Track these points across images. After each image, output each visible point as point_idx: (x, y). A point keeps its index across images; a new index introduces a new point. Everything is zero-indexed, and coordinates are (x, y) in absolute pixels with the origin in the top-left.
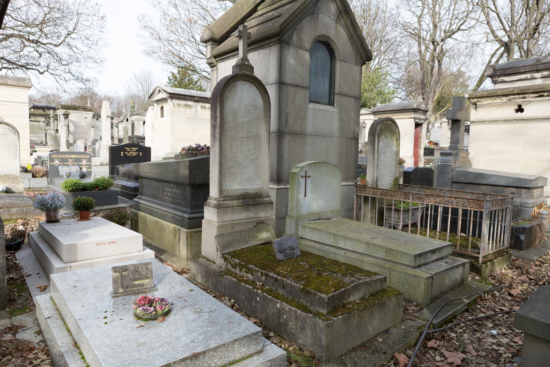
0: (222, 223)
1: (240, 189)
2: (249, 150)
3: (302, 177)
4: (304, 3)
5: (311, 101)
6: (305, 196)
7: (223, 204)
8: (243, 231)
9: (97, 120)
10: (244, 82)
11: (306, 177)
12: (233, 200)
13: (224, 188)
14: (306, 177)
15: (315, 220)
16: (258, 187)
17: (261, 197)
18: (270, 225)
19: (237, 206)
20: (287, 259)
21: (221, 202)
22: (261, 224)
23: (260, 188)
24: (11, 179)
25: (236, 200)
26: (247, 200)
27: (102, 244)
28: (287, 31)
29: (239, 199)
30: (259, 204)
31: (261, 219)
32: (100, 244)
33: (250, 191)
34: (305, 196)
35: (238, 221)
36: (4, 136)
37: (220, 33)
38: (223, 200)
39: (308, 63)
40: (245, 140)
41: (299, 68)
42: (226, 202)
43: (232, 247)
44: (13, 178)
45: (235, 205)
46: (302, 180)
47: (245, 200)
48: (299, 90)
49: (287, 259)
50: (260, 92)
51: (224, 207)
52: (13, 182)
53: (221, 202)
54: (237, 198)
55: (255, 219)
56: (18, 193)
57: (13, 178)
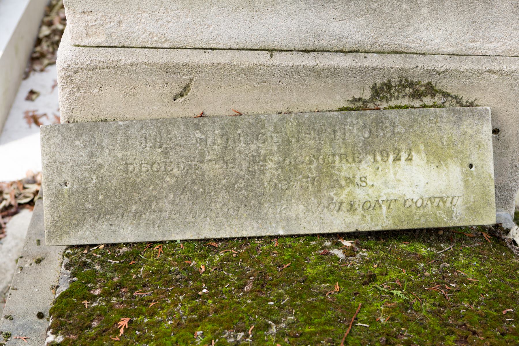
0: (101, 55)
18: (481, 116)
22: (417, 95)
31: (420, 62)
35: (225, 58)
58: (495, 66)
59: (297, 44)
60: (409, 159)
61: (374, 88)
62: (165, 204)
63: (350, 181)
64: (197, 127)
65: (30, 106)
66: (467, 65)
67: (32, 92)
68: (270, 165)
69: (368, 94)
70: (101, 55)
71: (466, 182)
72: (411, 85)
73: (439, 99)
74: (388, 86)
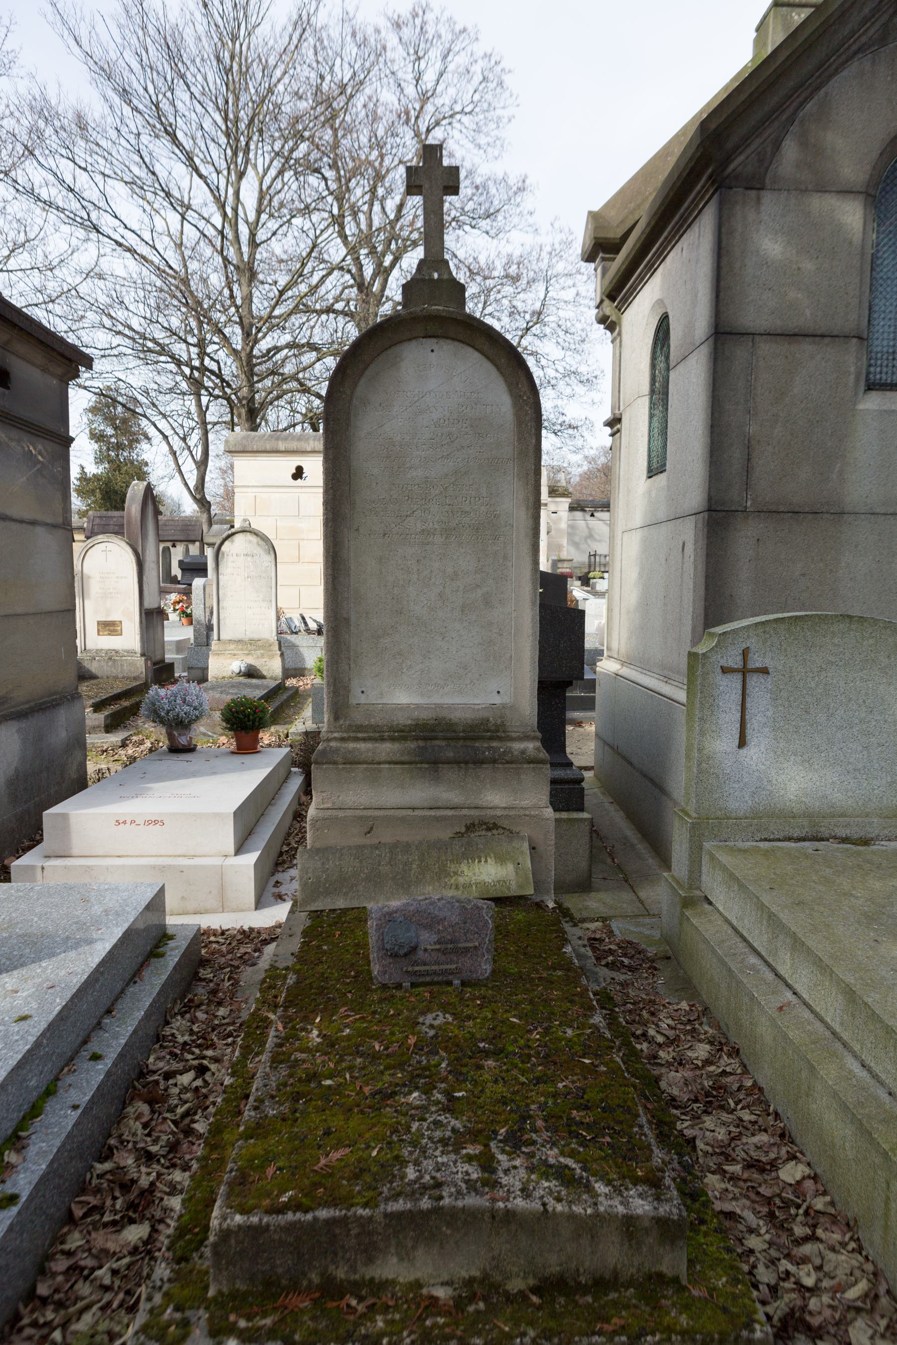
0: (329, 813)
1: (418, 707)
2: (456, 574)
3: (725, 670)
4: (842, 5)
5: (871, 387)
6: (742, 743)
7: (337, 750)
8: (408, 845)
9: (592, 515)
10: (431, 343)
11: (745, 672)
12: (382, 739)
13: (357, 698)
14: (745, 672)
15: (789, 839)
16: (497, 700)
17: (500, 739)
18: (523, 838)
19: (389, 763)
20: (413, 985)
21: (333, 744)
22: (489, 829)
23: (504, 706)
24: (259, 648)
25: (393, 739)
26: (437, 742)
27: (128, 822)
28: (746, 140)
29: (405, 738)
30: (482, 762)
31: (490, 813)
32: (125, 822)
33: (456, 716)
34: (742, 743)
35: (391, 812)
36: (249, 559)
37: (626, 217)
38: (342, 739)
39: (857, 237)
40: (438, 539)
41: (808, 266)
42: (351, 745)
43: (346, 894)
44: (263, 647)
45: (383, 757)
46: (729, 687)
47: (429, 743)
48: (807, 347)
49: (413, 985)
50: (498, 368)
51: (340, 760)
52: (262, 656)
53: (333, 744)
54: (399, 734)
55: (465, 812)
56: (271, 678)
57: (263, 647)
58: (527, 813)
59: (426, 805)
60: (486, 861)
61: (466, 826)
62: (360, 888)
63: (456, 873)
64: (377, 848)
65: (276, 890)
66: (512, 813)
67: (277, 882)
68: (414, 866)
69: (463, 830)
70: (329, 813)
71: (517, 873)
72: (485, 824)
73: (501, 831)
74: (473, 825)
